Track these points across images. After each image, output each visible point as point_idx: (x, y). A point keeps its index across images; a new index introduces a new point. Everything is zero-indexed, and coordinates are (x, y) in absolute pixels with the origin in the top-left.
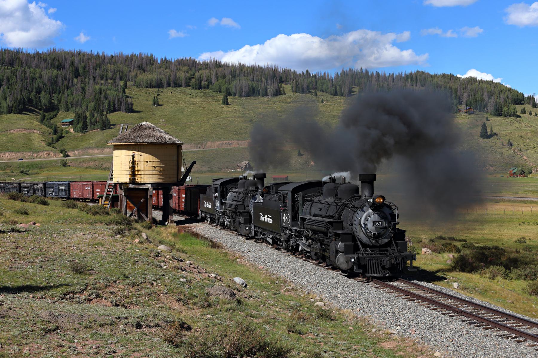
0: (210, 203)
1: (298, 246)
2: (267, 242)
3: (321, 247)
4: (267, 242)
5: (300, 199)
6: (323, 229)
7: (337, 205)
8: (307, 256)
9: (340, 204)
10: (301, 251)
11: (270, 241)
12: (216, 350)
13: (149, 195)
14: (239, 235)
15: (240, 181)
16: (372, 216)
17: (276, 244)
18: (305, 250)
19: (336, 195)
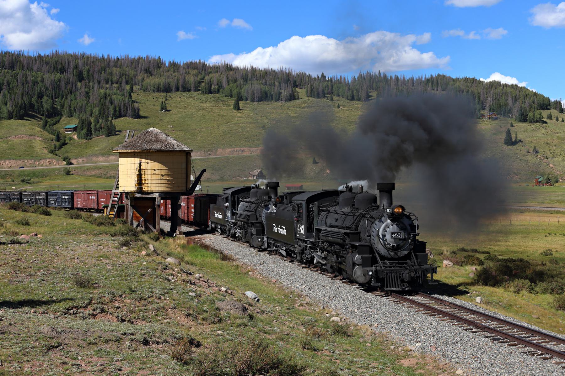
0: (221, 213)
1: (313, 258)
2: (281, 255)
3: (338, 259)
4: (281, 255)
5: (315, 209)
6: (339, 241)
7: (354, 215)
8: (322, 269)
9: (357, 214)
10: (316, 263)
11: (284, 253)
12: (227, 368)
13: (157, 205)
14: (251, 247)
15: (252, 190)
16: (391, 227)
17: (290, 256)
18: (320, 263)
19: (353, 205)
